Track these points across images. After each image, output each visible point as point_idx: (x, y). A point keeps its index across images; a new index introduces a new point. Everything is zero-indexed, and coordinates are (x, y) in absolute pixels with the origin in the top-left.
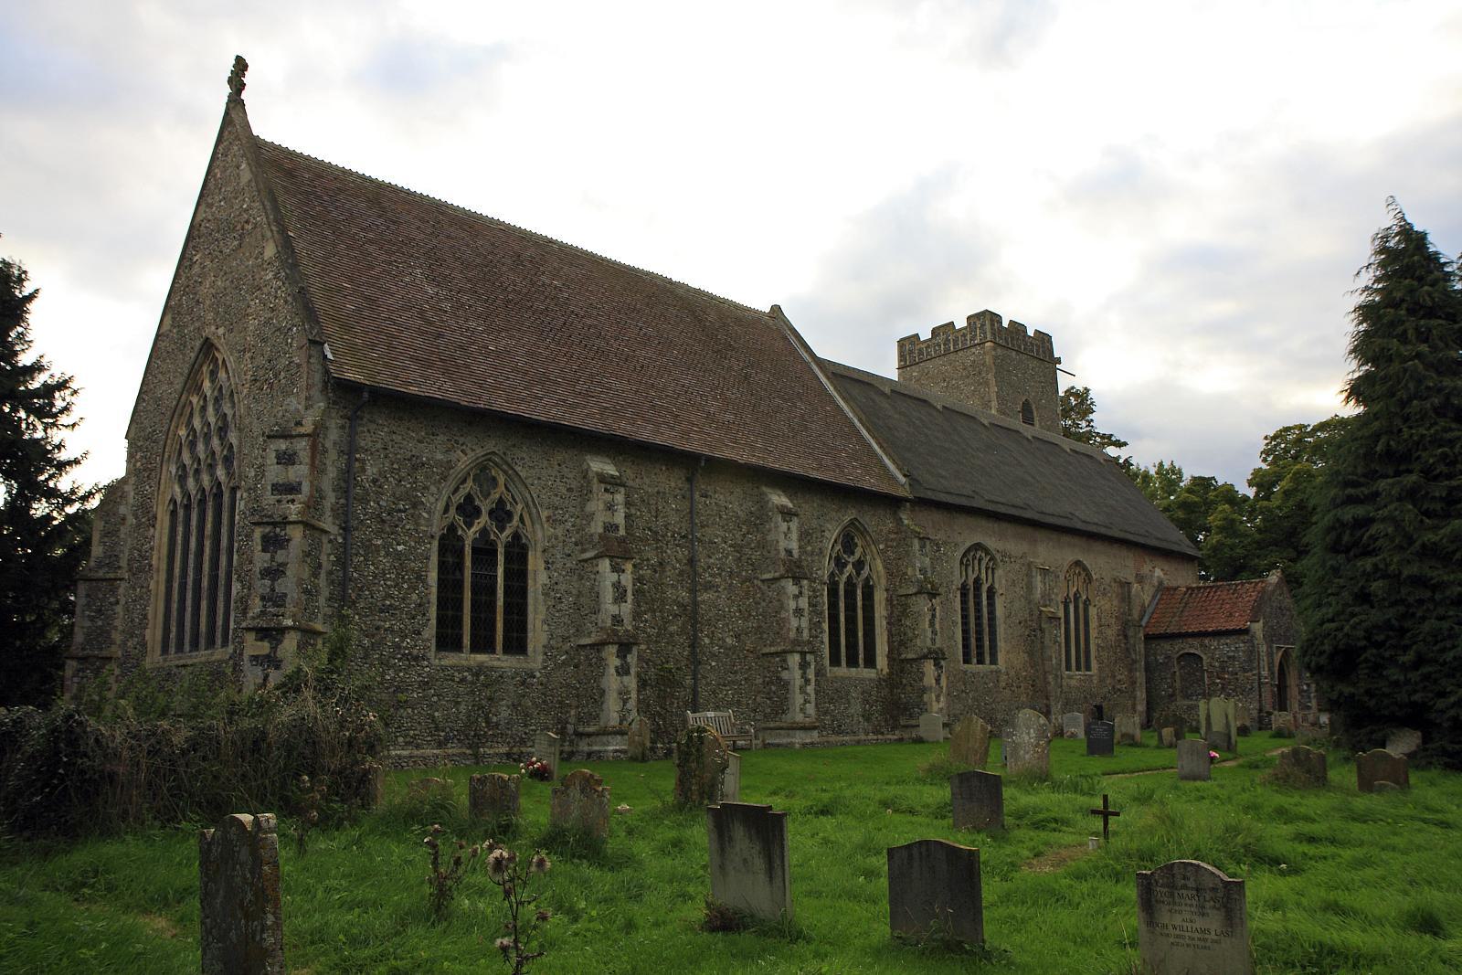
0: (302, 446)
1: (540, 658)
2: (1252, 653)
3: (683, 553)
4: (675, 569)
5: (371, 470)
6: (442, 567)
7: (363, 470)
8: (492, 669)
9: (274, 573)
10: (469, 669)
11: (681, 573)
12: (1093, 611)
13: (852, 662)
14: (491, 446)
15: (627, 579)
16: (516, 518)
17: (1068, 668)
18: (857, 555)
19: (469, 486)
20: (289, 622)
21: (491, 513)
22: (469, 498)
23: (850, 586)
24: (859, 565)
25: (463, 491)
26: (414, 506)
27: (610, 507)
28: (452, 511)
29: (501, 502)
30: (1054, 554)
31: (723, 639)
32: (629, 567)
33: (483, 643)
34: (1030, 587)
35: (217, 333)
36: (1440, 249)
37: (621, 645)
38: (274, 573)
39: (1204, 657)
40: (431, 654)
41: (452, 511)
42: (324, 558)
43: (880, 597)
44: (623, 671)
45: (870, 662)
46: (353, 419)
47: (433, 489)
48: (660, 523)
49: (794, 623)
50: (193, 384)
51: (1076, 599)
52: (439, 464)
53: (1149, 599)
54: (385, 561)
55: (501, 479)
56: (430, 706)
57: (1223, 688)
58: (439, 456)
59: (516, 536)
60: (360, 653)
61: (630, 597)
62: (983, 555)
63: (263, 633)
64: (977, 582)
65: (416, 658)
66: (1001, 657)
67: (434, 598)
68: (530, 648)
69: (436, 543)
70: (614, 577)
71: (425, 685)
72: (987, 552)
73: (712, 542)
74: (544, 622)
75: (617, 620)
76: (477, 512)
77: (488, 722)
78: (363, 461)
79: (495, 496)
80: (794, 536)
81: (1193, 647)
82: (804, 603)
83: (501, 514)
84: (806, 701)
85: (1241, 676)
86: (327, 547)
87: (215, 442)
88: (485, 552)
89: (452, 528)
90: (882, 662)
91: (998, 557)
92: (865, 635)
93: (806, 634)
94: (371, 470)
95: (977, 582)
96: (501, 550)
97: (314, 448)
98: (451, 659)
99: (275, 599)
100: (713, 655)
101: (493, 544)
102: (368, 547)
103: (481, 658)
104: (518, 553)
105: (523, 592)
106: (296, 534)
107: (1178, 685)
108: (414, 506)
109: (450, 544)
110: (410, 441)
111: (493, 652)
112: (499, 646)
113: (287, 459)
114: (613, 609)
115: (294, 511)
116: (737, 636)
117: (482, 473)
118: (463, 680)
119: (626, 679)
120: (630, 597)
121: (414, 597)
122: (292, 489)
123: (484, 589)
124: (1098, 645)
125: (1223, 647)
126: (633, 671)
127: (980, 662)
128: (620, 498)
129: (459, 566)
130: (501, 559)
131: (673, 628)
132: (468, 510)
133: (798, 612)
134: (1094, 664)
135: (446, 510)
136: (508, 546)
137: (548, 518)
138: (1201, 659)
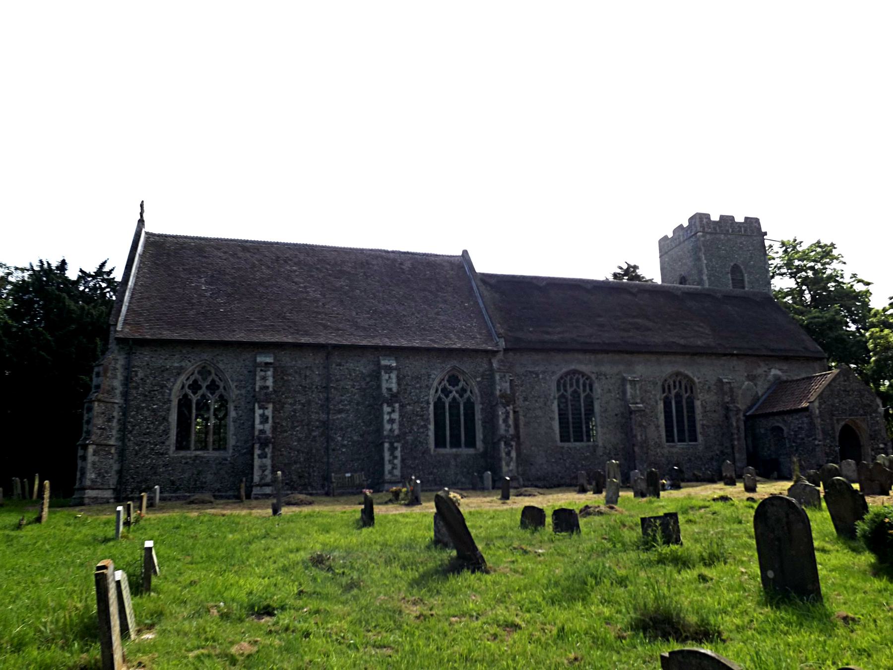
1: (231, 451)
2: (812, 424)
4: (317, 404)
5: (141, 374)
7: (136, 375)
8: (203, 457)
10: (190, 458)
11: (322, 406)
12: (698, 403)
13: (456, 443)
14: (205, 356)
15: (269, 412)
19: (196, 376)
22: (195, 381)
23: (454, 404)
25: (192, 378)
26: (162, 388)
27: (264, 378)
28: (439, 392)
31: (351, 438)
32: (271, 406)
34: (624, 392)
37: (261, 444)
39: (784, 428)
41: (439, 392)
43: (478, 408)
44: (263, 456)
45: (471, 443)
46: (129, 354)
47: (172, 380)
48: (308, 381)
49: (387, 427)
52: (176, 368)
53: (763, 391)
54: (145, 412)
55: (213, 371)
56: (169, 474)
57: (797, 450)
58: (176, 365)
60: (134, 452)
61: (270, 420)
62: (580, 376)
65: (162, 454)
70: (261, 411)
71: (165, 466)
72: (583, 374)
73: (343, 388)
74: (234, 435)
75: (262, 432)
76: (200, 387)
78: (136, 372)
80: (394, 380)
81: (777, 422)
82: (396, 416)
84: (393, 468)
85: (806, 440)
89: (439, 398)
90: (479, 444)
91: (593, 377)
94: (141, 374)
100: (344, 446)
102: (139, 409)
107: (773, 448)
108: (162, 388)
109: (439, 405)
110: (161, 359)
114: (261, 427)
116: (362, 436)
117: (204, 372)
118: (186, 463)
119: (264, 460)
120: (270, 420)
121: (162, 427)
124: (703, 425)
125: (794, 422)
126: (269, 455)
128: (270, 373)
131: (314, 434)
132: (195, 387)
133: (391, 421)
134: (700, 438)
135: (437, 391)
136: (450, 403)
137: (236, 386)
138: (782, 430)
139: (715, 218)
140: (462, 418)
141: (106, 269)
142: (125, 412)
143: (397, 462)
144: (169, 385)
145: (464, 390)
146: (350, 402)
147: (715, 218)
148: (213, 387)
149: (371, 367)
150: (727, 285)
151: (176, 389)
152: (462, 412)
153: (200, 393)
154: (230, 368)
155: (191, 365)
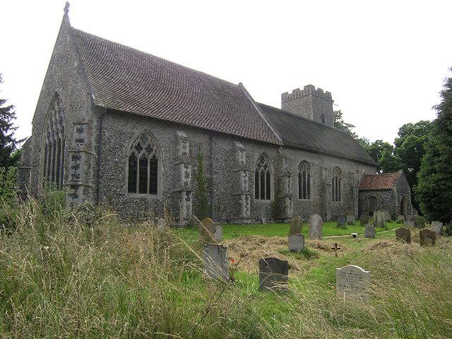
2: (393, 196)
22: (139, 144)
43: (272, 177)
44: (188, 200)
45: (268, 198)
72: (307, 163)
75: (186, 184)
76: (141, 148)
82: (247, 179)
90: (272, 198)
117: (143, 137)
120: (190, 176)
132: (139, 148)
133: (245, 181)
139: (302, 89)
140: (149, 182)
141: (11, 112)
142: (98, 164)
143: (249, 206)
144: (126, 145)
145: (266, 166)
146: (221, 167)
147: (290, 92)
148: (149, 149)
149: (230, 147)
150: (320, 121)
151: (128, 149)
152: (149, 177)
153: (142, 152)
154: (162, 138)
155: (138, 130)
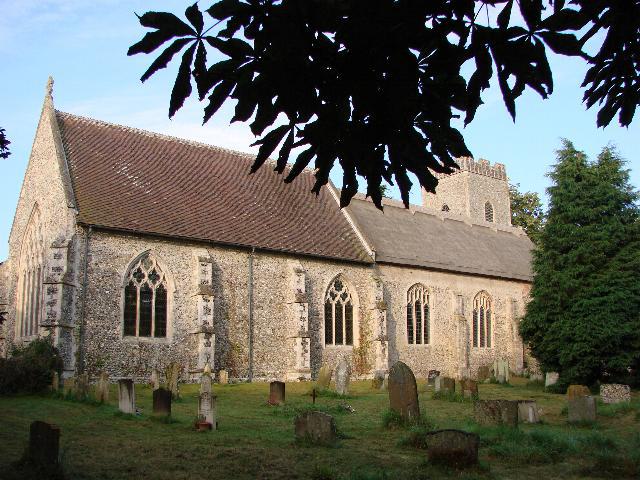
0: (64, 252)
3: (246, 292)
6: (127, 299)
9: (52, 304)
15: (211, 305)
16: (162, 278)
17: (475, 344)
18: (343, 291)
20: (56, 323)
21: (150, 276)
22: (139, 270)
23: (338, 305)
24: (344, 296)
28: (132, 276)
29: (154, 271)
30: (464, 285)
32: (212, 298)
33: (145, 332)
35: (39, 199)
36: (486, 157)
38: (52, 304)
40: (121, 336)
41: (132, 276)
42: (74, 297)
45: (349, 341)
50: (31, 220)
51: (482, 311)
59: (161, 286)
60: (89, 336)
61: (212, 312)
63: (48, 327)
64: (418, 303)
66: (431, 340)
67: (122, 313)
68: (168, 334)
69: (124, 290)
70: (205, 304)
77: (147, 365)
79: (151, 269)
83: (154, 276)
86: (75, 293)
87: (39, 246)
88: (147, 292)
92: (347, 329)
93: (306, 329)
95: (418, 303)
96: (154, 292)
97: (69, 253)
98: (129, 339)
99: (52, 314)
101: (331, 305)
103: (144, 339)
104: (349, 309)
105: (164, 310)
106: (60, 287)
111: (134, 334)
112: (153, 334)
113: (58, 257)
115: (59, 278)
122: (59, 269)
123: (146, 309)
127: (418, 342)
129: (135, 299)
130: (154, 296)
